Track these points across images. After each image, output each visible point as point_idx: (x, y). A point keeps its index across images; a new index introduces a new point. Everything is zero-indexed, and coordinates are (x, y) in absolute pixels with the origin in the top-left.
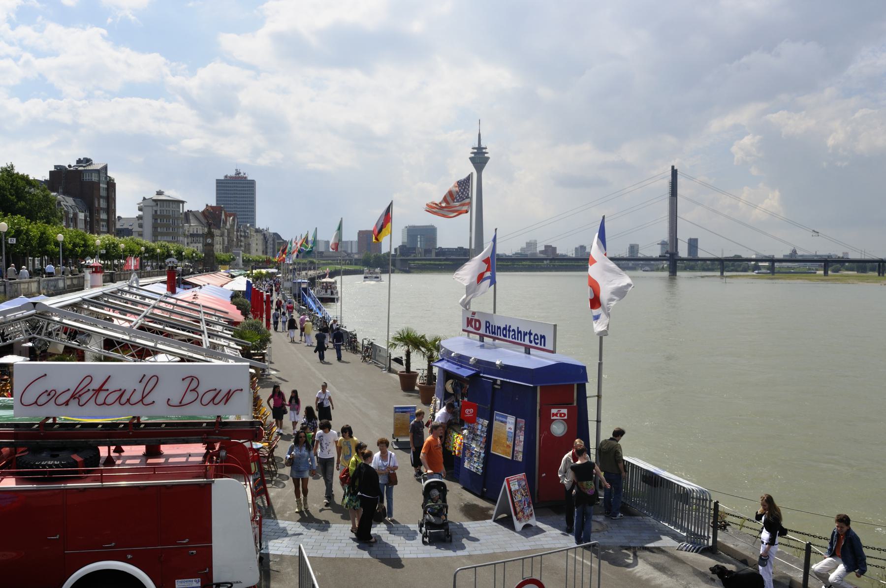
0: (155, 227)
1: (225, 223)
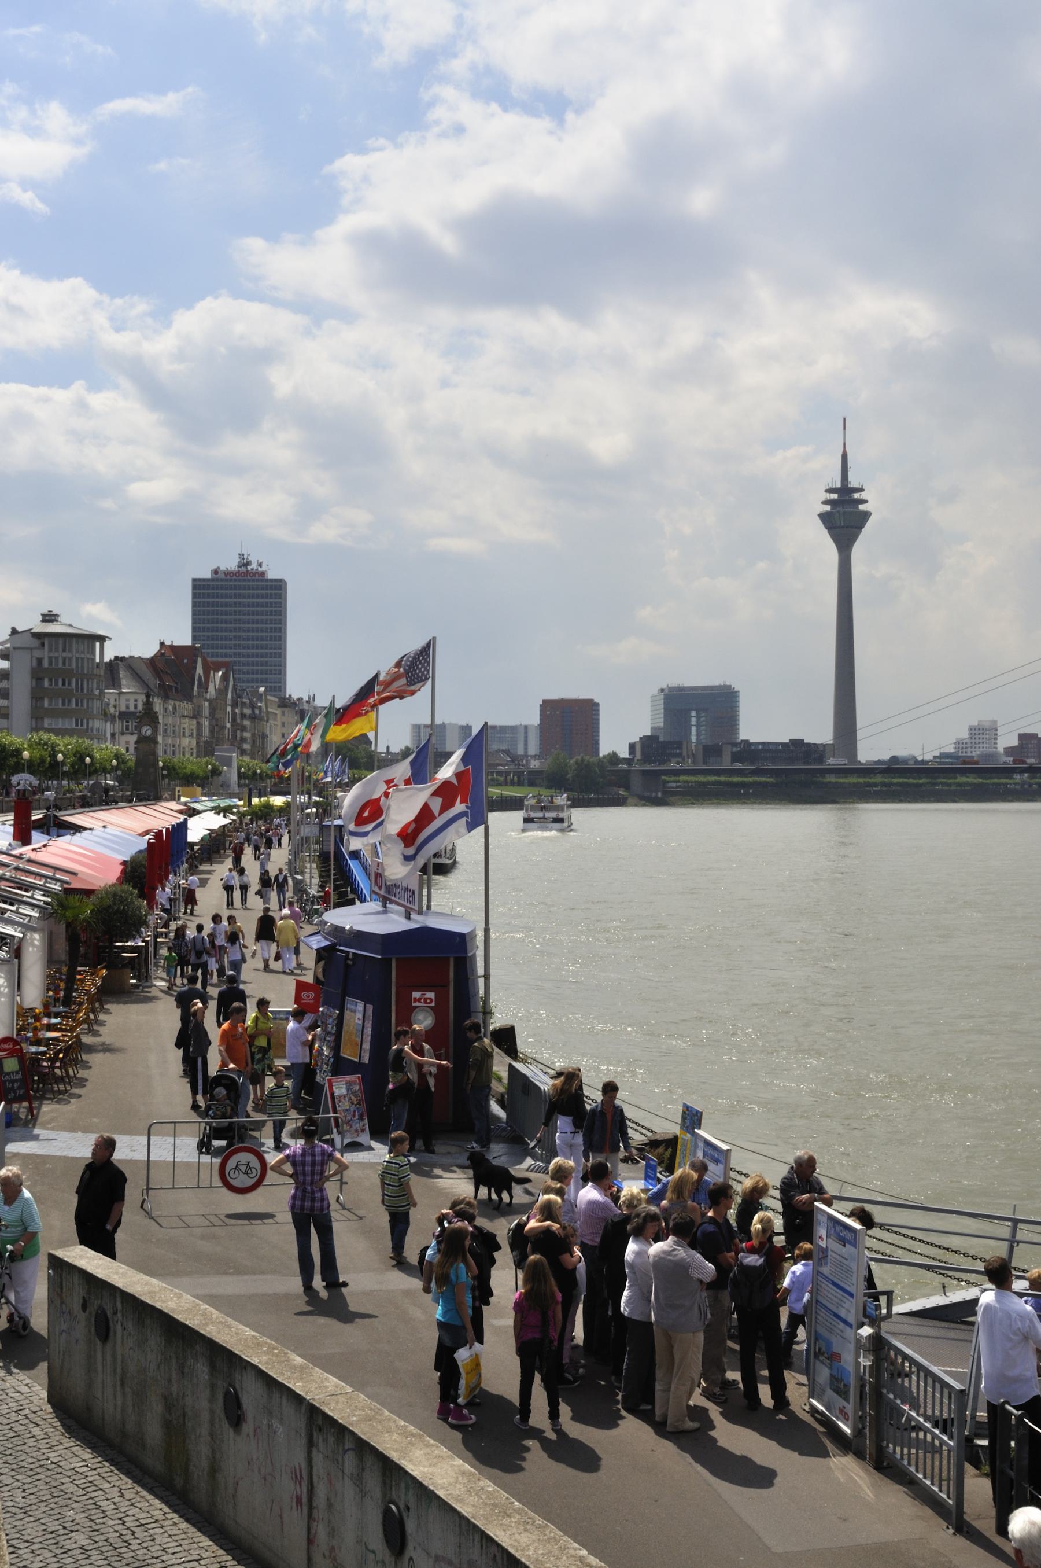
0: (37, 695)
1: (204, 686)
